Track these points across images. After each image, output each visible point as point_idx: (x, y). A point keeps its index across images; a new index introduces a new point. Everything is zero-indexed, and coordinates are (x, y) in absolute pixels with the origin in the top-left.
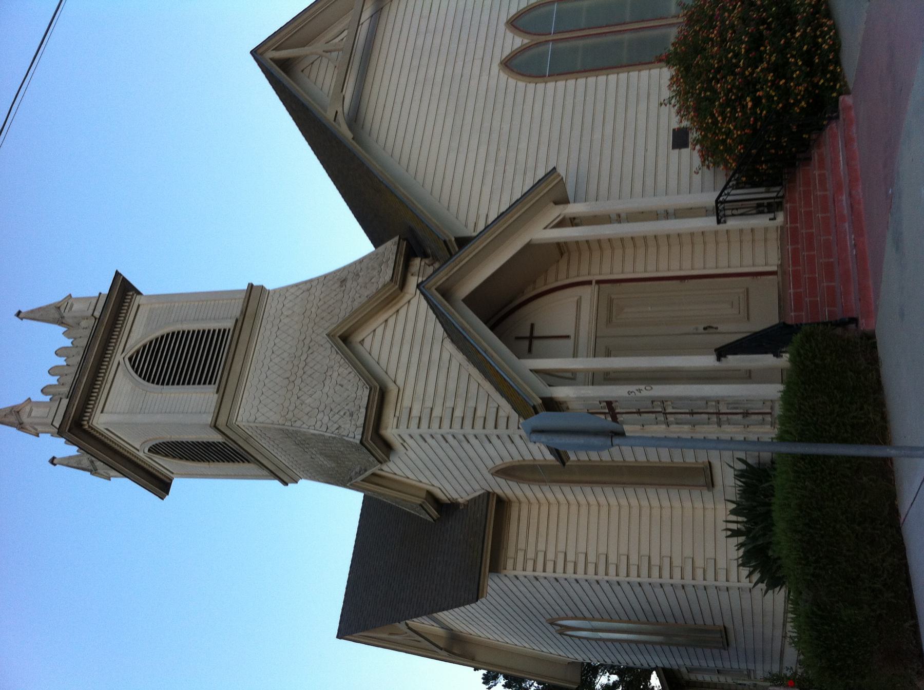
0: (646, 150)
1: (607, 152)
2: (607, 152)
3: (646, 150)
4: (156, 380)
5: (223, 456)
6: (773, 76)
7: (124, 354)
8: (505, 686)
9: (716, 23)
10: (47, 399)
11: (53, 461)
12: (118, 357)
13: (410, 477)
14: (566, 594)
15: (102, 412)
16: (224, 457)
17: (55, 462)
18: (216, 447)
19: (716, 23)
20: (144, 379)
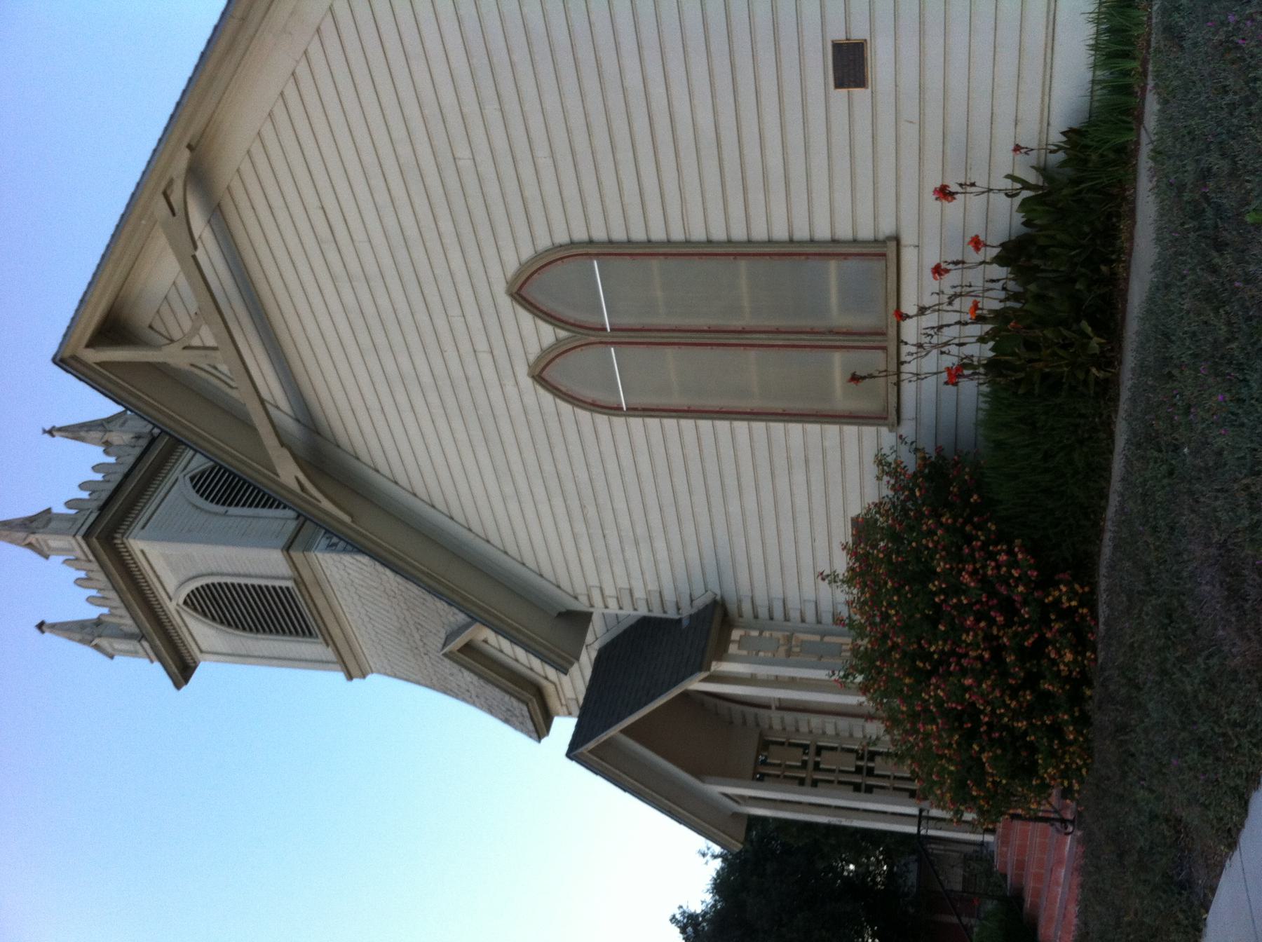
0: (813, 540)
1: (754, 533)
2: (754, 533)
3: (813, 540)
4: (206, 494)
5: (256, 597)
6: (1048, 716)
7: (184, 473)
8: (573, 752)
9: (937, 725)
10: (73, 512)
11: (41, 626)
12: (177, 472)
13: (381, 470)
14: (378, 446)
15: (143, 527)
16: (261, 595)
17: (44, 628)
18: (224, 609)
19: (937, 725)
20: (198, 492)
